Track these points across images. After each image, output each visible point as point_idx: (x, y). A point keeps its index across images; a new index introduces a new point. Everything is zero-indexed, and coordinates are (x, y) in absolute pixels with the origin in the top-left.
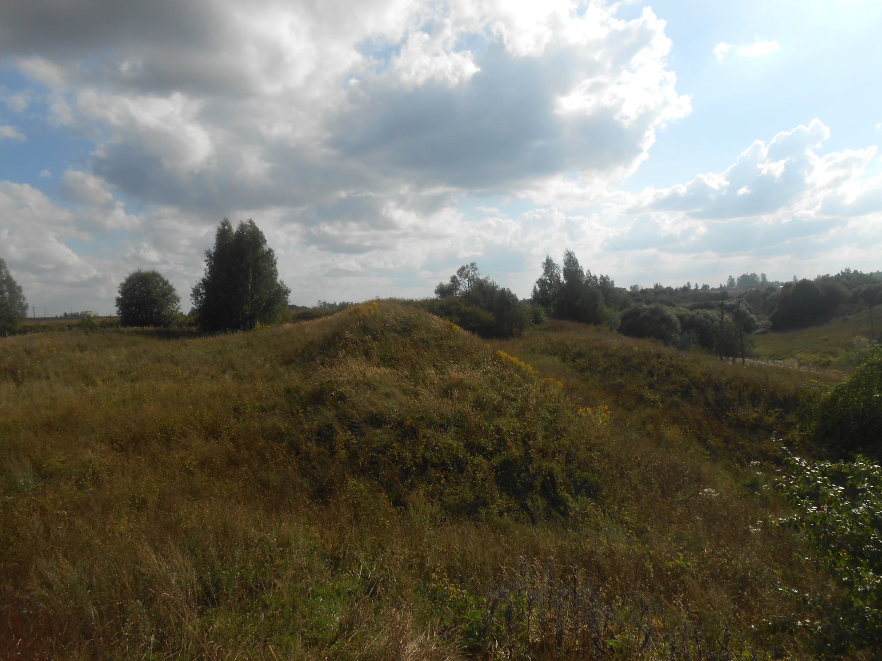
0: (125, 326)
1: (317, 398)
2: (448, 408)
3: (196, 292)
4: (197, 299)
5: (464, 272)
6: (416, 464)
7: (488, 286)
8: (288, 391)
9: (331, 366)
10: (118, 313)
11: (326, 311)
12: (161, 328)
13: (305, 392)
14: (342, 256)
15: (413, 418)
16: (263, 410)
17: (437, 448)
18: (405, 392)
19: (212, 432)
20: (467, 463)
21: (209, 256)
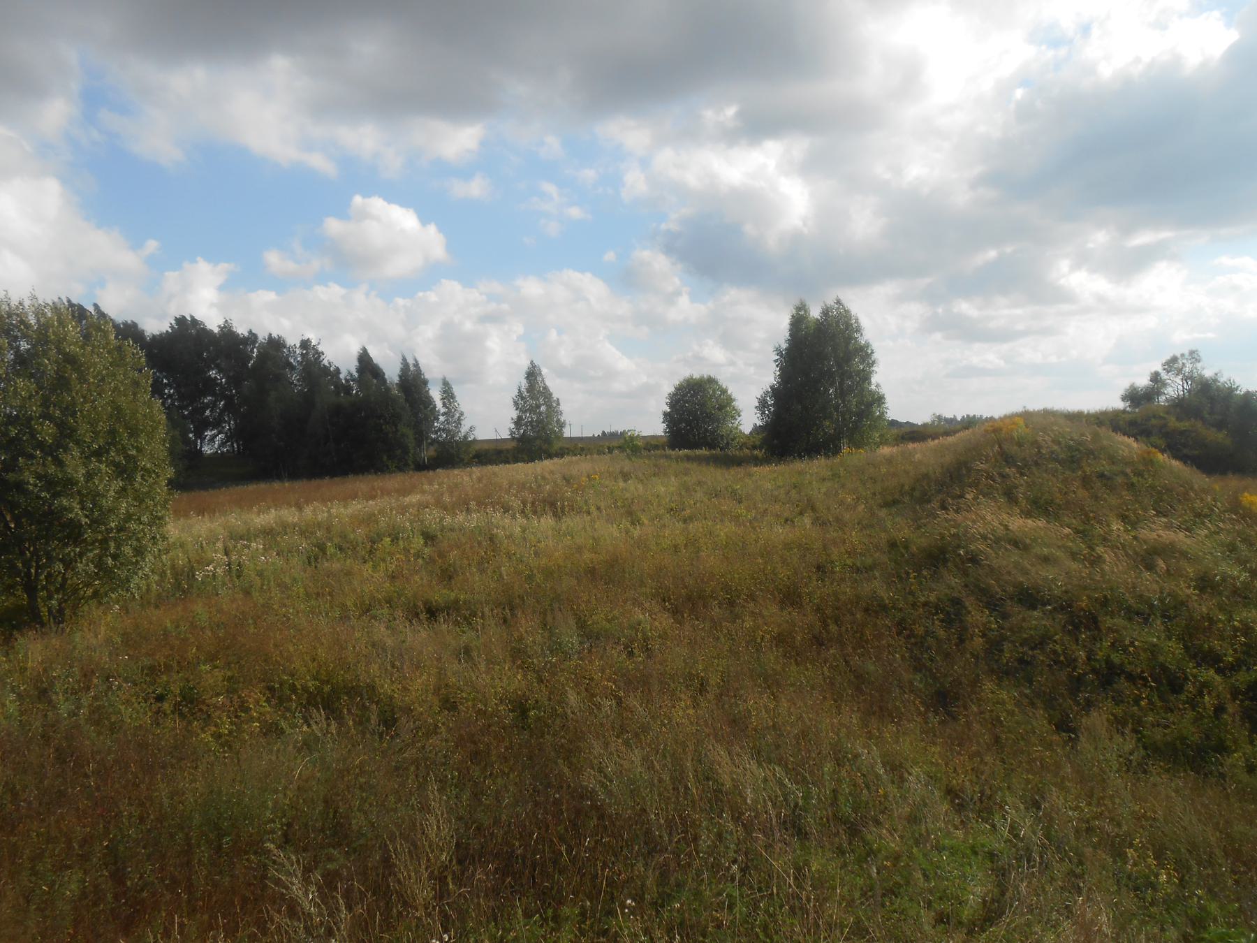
0: (673, 450)
1: (936, 558)
2: (1149, 584)
3: (762, 404)
4: (763, 413)
5: (1176, 365)
6: (1094, 671)
7: (1218, 387)
8: (893, 545)
9: (957, 511)
10: (665, 432)
11: (941, 429)
12: (717, 451)
13: (917, 549)
14: (977, 346)
15: (1089, 597)
16: (858, 570)
17: (1131, 649)
18: (1074, 556)
19: (790, 597)
20: (1186, 679)
21: (780, 354)
